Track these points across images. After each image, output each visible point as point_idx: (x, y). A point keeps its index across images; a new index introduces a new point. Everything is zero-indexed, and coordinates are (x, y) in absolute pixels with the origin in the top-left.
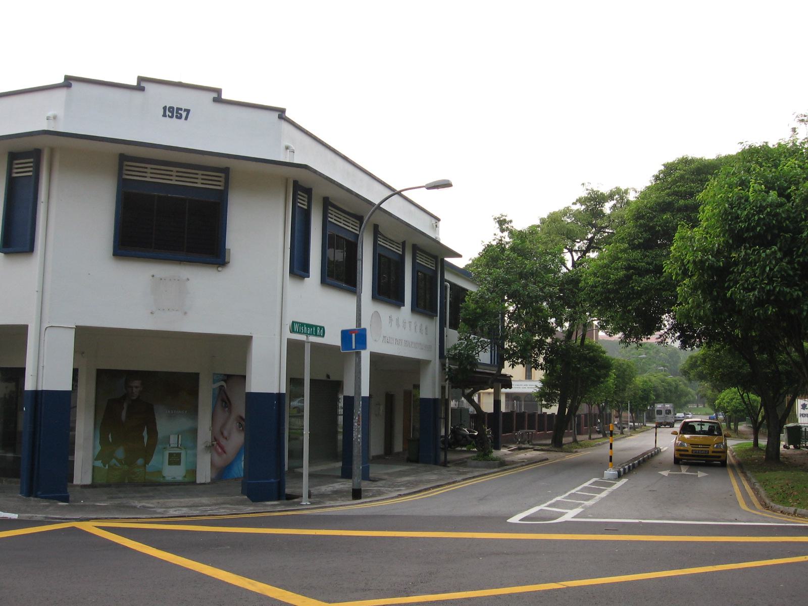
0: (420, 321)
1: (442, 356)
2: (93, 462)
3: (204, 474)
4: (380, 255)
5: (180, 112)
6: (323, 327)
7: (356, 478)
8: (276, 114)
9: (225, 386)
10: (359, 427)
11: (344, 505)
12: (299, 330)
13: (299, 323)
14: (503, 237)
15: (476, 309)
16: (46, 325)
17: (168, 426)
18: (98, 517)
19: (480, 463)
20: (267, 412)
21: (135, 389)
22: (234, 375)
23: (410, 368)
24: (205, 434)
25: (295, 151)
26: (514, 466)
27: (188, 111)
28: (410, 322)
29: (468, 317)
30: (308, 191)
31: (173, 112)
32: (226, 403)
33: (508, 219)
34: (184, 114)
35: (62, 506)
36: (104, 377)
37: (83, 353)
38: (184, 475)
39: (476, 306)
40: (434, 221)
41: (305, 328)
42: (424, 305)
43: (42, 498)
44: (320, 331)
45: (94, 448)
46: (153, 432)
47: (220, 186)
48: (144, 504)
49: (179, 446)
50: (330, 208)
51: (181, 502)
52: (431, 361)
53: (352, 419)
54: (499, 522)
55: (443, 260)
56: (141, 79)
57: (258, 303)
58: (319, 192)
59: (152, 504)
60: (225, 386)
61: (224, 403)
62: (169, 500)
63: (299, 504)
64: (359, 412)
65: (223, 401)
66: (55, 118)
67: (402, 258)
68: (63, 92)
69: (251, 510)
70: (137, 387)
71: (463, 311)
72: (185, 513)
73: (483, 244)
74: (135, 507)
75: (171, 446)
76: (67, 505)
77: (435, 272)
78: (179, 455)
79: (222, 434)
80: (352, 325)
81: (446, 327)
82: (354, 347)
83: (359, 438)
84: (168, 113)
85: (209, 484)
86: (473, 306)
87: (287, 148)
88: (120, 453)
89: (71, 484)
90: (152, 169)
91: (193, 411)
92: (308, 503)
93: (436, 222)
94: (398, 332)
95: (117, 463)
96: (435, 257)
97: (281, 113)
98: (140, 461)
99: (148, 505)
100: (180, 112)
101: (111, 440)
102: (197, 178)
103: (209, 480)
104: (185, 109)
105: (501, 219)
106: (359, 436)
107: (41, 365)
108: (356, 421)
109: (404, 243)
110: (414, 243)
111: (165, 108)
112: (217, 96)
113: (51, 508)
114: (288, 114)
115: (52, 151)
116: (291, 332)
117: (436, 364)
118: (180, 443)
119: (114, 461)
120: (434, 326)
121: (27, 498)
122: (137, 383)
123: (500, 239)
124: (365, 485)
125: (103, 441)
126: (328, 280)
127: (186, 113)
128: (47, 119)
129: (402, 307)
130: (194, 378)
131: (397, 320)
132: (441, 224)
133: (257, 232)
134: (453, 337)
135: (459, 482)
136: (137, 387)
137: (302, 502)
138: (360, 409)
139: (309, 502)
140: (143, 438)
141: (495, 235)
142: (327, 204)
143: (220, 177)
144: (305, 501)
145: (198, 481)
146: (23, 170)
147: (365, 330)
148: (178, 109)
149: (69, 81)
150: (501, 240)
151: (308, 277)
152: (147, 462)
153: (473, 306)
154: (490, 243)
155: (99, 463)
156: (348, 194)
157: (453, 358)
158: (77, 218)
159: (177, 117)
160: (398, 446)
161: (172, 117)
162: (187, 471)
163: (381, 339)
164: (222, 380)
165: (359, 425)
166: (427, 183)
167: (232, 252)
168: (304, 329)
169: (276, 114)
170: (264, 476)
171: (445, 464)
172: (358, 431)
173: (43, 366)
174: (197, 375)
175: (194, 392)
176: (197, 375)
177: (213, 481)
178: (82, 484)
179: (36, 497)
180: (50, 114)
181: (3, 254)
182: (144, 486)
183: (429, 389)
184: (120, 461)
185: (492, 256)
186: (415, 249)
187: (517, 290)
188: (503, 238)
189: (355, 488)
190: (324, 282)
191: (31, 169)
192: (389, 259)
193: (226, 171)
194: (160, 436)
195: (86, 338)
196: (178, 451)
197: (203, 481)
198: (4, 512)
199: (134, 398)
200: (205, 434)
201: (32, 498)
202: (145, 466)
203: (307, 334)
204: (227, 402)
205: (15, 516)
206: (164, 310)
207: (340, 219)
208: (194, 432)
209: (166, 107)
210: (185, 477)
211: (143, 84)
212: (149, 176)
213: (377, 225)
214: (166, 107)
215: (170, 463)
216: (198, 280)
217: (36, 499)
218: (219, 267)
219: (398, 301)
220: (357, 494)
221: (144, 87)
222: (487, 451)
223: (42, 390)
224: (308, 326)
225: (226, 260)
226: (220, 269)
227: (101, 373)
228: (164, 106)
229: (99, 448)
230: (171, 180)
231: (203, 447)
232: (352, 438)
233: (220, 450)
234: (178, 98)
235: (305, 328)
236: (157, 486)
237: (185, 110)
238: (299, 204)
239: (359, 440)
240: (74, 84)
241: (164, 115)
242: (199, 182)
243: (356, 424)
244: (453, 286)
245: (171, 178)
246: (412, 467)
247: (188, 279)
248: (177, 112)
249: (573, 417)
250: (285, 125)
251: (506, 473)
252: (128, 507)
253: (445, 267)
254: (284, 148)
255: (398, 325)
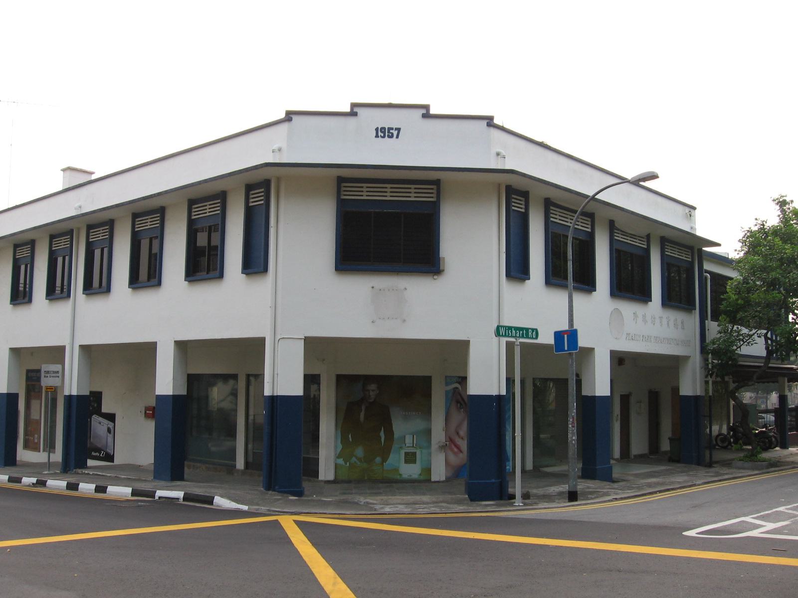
0: (674, 316)
1: (704, 350)
2: (336, 460)
3: (439, 472)
4: (618, 251)
5: (391, 131)
6: (536, 330)
7: (571, 481)
8: (485, 122)
9: (460, 389)
10: (573, 429)
11: (548, 508)
12: (505, 333)
13: (506, 327)
14: (764, 221)
15: (737, 300)
16: (278, 337)
17: (403, 427)
18: (309, 512)
19: (746, 465)
20: (488, 415)
21: (371, 393)
22: (237, 399)
23: (666, 367)
24: (438, 434)
25: (506, 157)
26: (782, 468)
27: (399, 130)
28: (661, 318)
29: (728, 309)
30: (525, 195)
31: (384, 133)
32: (461, 404)
33: (788, 199)
34: (395, 133)
35: (291, 500)
36: (343, 381)
37: (324, 360)
38: (420, 473)
39: (737, 297)
40: (687, 210)
41: (514, 331)
42: (678, 296)
43: (278, 492)
44: (532, 334)
45: (336, 447)
46: (390, 433)
47: (432, 197)
48: (368, 500)
49: (414, 445)
50: (552, 208)
51: (403, 499)
52: (690, 356)
53: (567, 421)
54: (671, 534)
55: (700, 251)
56: (354, 105)
57: (475, 306)
58: (537, 194)
59: (377, 500)
60: (460, 389)
61: (459, 405)
62: (393, 497)
63: (512, 505)
64: (573, 414)
65: (458, 402)
66: (280, 150)
67: (647, 251)
68: (285, 127)
69: (461, 509)
70: (373, 391)
71: (724, 303)
72: (394, 511)
73: (743, 230)
74: (357, 503)
75: (407, 445)
76: (296, 499)
77: (692, 264)
78: (414, 454)
79: (458, 433)
80: (566, 327)
81: (707, 320)
82: (566, 348)
83: (574, 440)
84: (380, 134)
85: (443, 482)
86: (734, 297)
87: (498, 154)
88: (360, 452)
89: (316, 479)
90: (367, 187)
91: (427, 412)
92: (521, 504)
93: (690, 211)
94: (653, 328)
95: (357, 461)
96: (691, 248)
97: (489, 121)
98: (378, 460)
99: (371, 501)
100: (391, 131)
101: (351, 440)
102: (410, 193)
103: (443, 478)
104: (396, 128)
105: (781, 200)
106: (574, 438)
107: (276, 373)
108: (571, 423)
109: (648, 237)
110: (662, 235)
111: (377, 129)
112: (426, 112)
113: (280, 501)
114: (496, 121)
115: (279, 179)
116: (496, 336)
117: (696, 358)
118: (415, 442)
119: (354, 459)
120: (694, 319)
121: (267, 492)
122: (373, 387)
123: (762, 223)
124: (583, 485)
125: (344, 440)
126: (552, 281)
127: (397, 131)
128: (273, 152)
129: (649, 303)
130: (426, 381)
131: (644, 316)
132: (697, 213)
133: (471, 240)
134: (713, 328)
135: (699, 485)
136: (373, 391)
137: (515, 503)
138: (575, 411)
139: (522, 503)
140: (380, 438)
141: (756, 219)
142: (549, 205)
143: (432, 189)
144: (518, 502)
145: (433, 479)
146: (257, 200)
147: (576, 331)
148: (390, 129)
149: (290, 116)
150: (763, 225)
151: (529, 279)
152: (385, 459)
153: (734, 297)
154: (750, 228)
155: (340, 461)
156: (567, 194)
157: (716, 353)
158: (305, 236)
159: (389, 137)
160: (665, 446)
161: (384, 137)
162: (423, 470)
163: (624, 336)
164: (457, 382)
165: (573, 427)
166: (632, 177)
167: (446, 260)
168: (512, 332)
169: (485, 122)
170: (485, 479)
171: (710, 465)
172: (573, 434)
173: (277, 374)
174: (430, 378)
175: (427, 395)
176: (430, 378)
177: (448, 480)
178: (326, 480)
179: (274, 490)
180: (276, 147)
181: (245, 275)
182: (382, 482)
183: (691, 384)
184: (360, 460)
185: (756, 241)
186: (664, 242)
187: (775, 279)
188: (764, 223)
189: (570, 490)
190: (548, 283)
191: (262, 198)
192: (632, 254)
193: (437, 183)
194: (396, 436)
195: (315, 347)
196: (412, 450)
197: (437, 480)
198: (238, 504)
199: (371, 401)
200: (438, 434)
201: (270, 492)
202: (382, 464)
203: (516, 336)
204: (462, 402)
205: (245, 508)
206: (384, 318)
207: (567, 218)
208: (428, 432)
209: (378, 128)
210: (420, 475)
211: (356, 110)
212: (365, 194)
213: (612, 220)
214: (378, 128)
215: (406, 462)
216: (415, 289)
217: (274, 493)
218: (435, 275)
219: (644, 295)
220: (573, 496)
221: (357, 112)
222: (755, 451)
223: (277, 396)
224: (517, 329)
225: (441, 269)
226: (435, 277)
227: (340, 378)
228: (376, 128)
229: (340, 447)
230: (386, 196)
231: (437, 446)
232: (568, 439)
233: (456, 450)
234: (387, 119)
235: (514, 331)
236: (392, 483)
237: (396, 129)
238: (513, 208)
239: (573, 442)
240: (295, 118)
241: (377, 136)
242: (412, 195)
243: (570, 426)
244: (715, 277)
245: (385, 194)
246: (668, 467)
247: (406, 289)
248: (389, 132)
249: (707, 423)
250: (493, 131)
251: (784, 473)
252: (350, 503)
253: (704, 257)
254: (495, 154)
255: (645, 321)
